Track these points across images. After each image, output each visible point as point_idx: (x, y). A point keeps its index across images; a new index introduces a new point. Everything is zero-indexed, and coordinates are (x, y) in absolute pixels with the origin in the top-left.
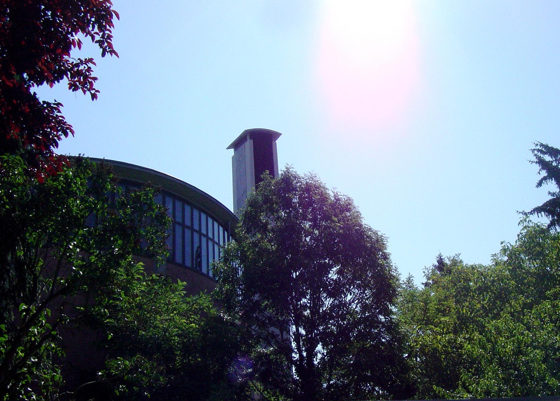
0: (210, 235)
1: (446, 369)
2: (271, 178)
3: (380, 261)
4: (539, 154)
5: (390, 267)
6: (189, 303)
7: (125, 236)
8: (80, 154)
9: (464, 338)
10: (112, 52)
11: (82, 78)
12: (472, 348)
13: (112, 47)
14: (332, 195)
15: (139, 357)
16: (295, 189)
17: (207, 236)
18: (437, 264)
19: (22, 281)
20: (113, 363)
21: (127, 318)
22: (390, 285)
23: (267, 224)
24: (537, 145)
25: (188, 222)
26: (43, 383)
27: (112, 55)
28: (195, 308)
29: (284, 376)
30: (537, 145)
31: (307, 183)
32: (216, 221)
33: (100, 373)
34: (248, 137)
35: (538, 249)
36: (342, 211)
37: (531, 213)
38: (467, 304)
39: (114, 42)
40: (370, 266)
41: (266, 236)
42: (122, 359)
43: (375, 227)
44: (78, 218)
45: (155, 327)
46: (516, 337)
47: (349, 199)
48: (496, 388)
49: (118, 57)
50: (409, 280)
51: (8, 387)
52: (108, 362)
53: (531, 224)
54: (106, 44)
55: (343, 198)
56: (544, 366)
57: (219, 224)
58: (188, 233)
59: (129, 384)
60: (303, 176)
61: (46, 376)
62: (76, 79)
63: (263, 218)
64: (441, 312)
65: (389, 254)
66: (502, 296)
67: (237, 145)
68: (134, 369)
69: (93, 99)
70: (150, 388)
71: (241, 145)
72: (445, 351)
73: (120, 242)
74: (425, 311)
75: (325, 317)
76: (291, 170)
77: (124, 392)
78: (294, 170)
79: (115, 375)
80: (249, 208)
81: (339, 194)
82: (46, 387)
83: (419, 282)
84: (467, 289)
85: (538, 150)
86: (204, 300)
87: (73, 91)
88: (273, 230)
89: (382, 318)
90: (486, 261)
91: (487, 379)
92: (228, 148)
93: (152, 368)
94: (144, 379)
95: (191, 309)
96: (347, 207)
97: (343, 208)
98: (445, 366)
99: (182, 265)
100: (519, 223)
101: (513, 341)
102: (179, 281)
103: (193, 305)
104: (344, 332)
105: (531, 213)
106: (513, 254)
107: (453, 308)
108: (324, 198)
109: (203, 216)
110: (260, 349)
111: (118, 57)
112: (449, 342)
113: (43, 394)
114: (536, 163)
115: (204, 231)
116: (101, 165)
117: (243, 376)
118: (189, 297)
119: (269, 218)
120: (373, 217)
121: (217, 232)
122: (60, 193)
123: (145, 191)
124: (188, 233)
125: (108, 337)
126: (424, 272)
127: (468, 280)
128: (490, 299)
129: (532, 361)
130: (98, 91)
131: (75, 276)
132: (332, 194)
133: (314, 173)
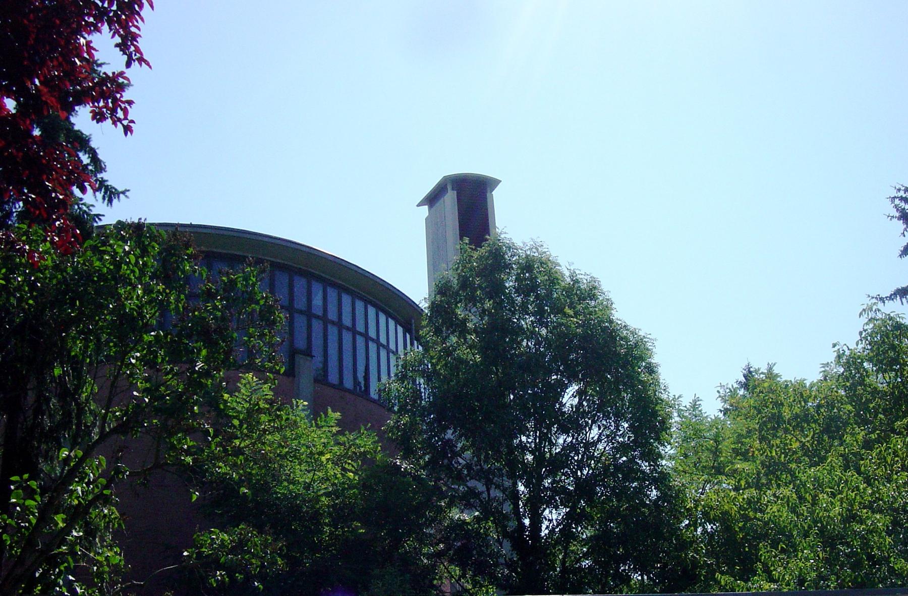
0: (383, 340)
1: (739, 547)
2: (472, 249)
3: (644, 377)
4: (903, 204)
5: (657, 383)
6: (343, 444)
7: (211, 344)
8: (140, 219)
9: (774, 495)
10: (141, 60)
11: (110, 101)
12: (778, 511)
13: (141, 54)
14: (567, 273)
15: (242, 529)
16: (509, 266)
17: (377, 341)
18: (743, 380)
19: (67, 414)
20: (205, 538)
21: (219, 467)
22: (655, 414)
23: (465, 321)
24: (899, 190)
25: (347, 321)
26: (95, 568)
27: (141, 65)
28: (354, 453)
29: (491, 556)
30: (899, 190)
31: (527, 256)
32: (393, 318)
33: (185, 554)
34: (449, 187)
35: (891, 354)
36: (582, 299)
37: (891, 297)
38: (778, 441)
39: (141, 43)
40: (625, 384)
41: (465, 339)
42: (217, 531)
43: (632, 324)
44: (134, 318)
45: (293, 482)
46: (845, 494)
47: (594, 280)
48: (814, 574)
49: (150, 67)
50: (695, 405)
51: (37, 575)
52: (198, 536)
53: (879, 316)
54: (132, 48)
55: (584, 280)
56: (888, 540)
57: (397, 322)
58: (347, 337)
59: (230, 570)
60: (521, 245)
61: (97, 558)
62: (101, 104)
63: (460, 312)
64: (741, 454)
65: (657, 365)
66: (833, 428)
67: (432, 199)
68: (239, 546)
69: (126, 134)
70: (262, 578)
71: (438, 200)
72: (743, 516)
73: (204, 352)
74: (715, 453)
75: (558, 463)
76: (502, 236)
77: (223, 581)
78: (506, 236)
79: (208, 556)
80: (438, 298)
81: (577, 272)
82: (100, 574)
83: (712, 408)
84: (777, 419)
85: (901, 199)
86: (366, 442)
87: (98, 122)
88: (475, 331)
89: (645, 466)
90: (811, 375)
91: (801, 560)
92: (418, 205)
93: (265, 545)
94: (254, 561)
95: (347, 453)
96: (591, 293)
97: (583, 295)
98: (742, 539)
99: (340, 387)
100: (861, 314)
101: (841, 500)
102: (330, 410)
103: (350, 447)
104: (585, 488)
105: (891, 297)
106: (852, 362)
107: (758, 450)
108: (553, 279)
109: (372, 311)
110: (455, 514)
111: (150, 67)
112: (749, 502)
113: (95, 585)
114: (899, 219)
115: (372, 333)
116: (174, 235)
117: (429, 556)
118: (344, 435)
119: (470, 311)
120: (631, 309)
121: (394, 334)
122: (106, 280)
123: (244, 272)
124: (347, 337)
125: (191, 498)
126: (718, 392)
127: (779, 404)
128: (814, 435)
129: (870, 532)
130: (132, 122)
131: (138, 405)
132: (567, 273)
133: (539, 240)
